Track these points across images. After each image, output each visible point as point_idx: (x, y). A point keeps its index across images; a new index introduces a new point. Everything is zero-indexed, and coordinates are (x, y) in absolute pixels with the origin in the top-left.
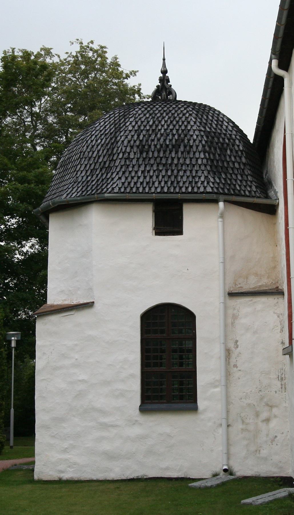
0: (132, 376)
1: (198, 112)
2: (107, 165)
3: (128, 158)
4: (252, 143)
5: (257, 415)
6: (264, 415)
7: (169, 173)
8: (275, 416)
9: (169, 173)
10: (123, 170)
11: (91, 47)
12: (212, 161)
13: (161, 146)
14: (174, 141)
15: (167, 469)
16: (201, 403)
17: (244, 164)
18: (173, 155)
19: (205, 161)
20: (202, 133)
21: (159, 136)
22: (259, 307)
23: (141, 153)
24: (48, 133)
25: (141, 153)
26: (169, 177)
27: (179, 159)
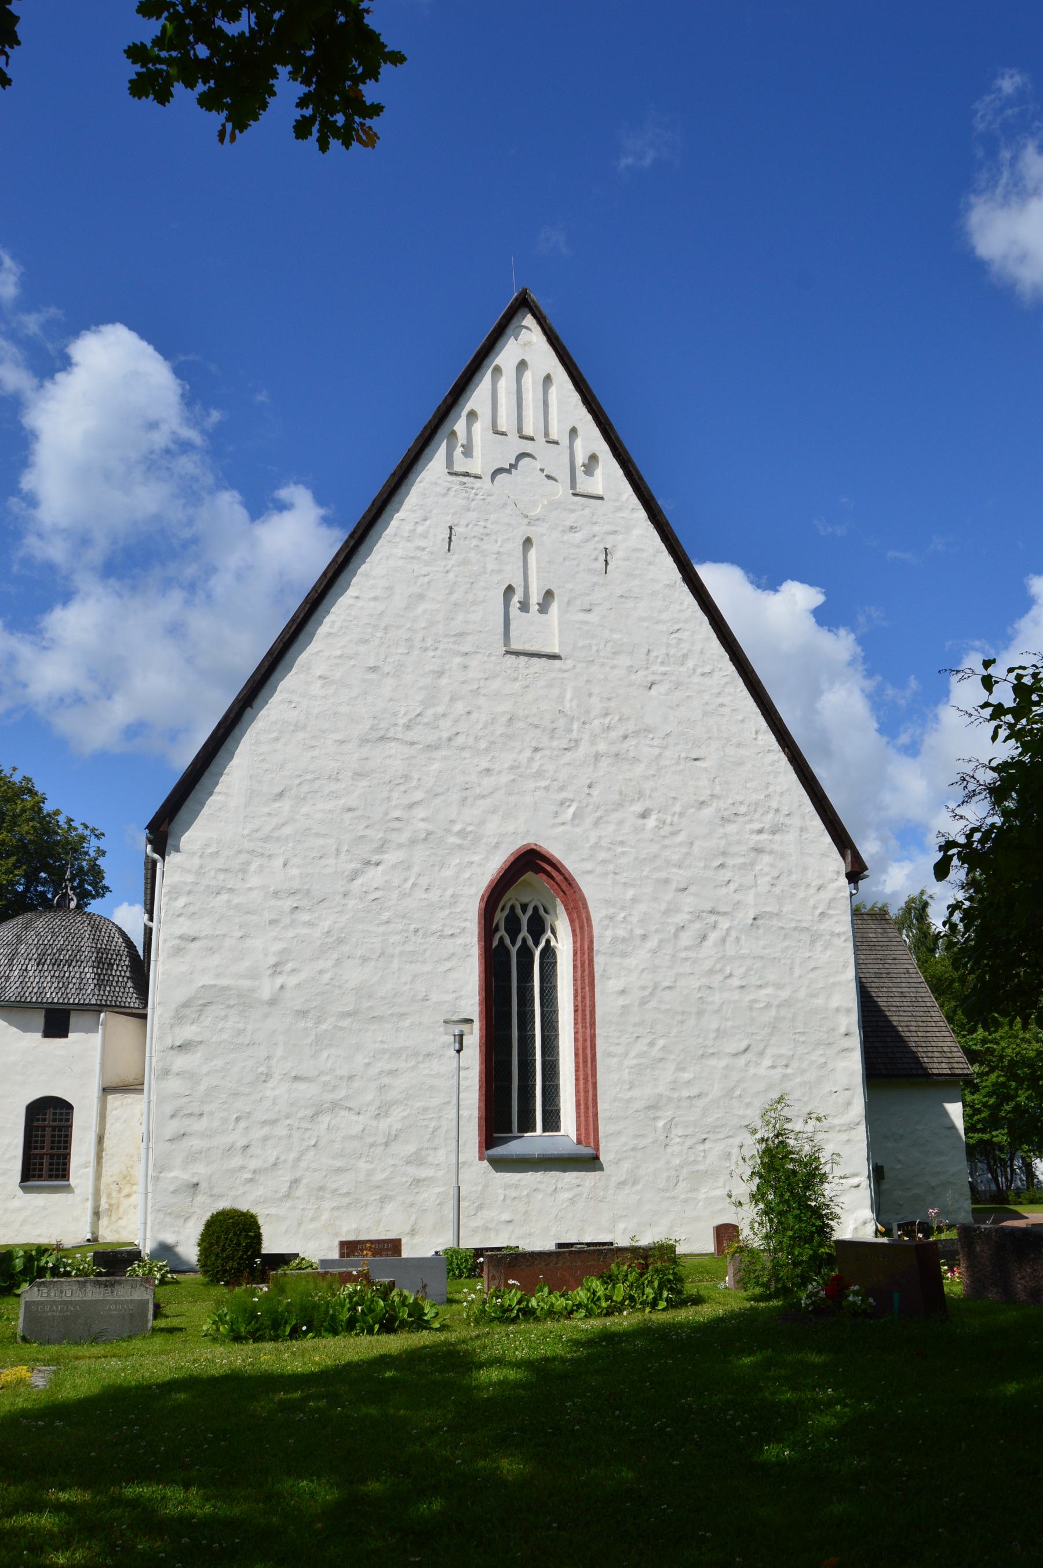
0: (15, 1157)
1: (92, 928)
2: (6, 974)
3: (26, 970)
4: (276, 66)
5: (120, 1191)
6: (125, 1192)
7: (61, 985)
8: (135, 1192)
9: (61, 985)
10: (20, 980)
11: (298, 105)
12: (99, 975)
13: (56, 960)
14: (67, 956)
15: (39, 1236)
16: (73, 1180)
17: (128, 978)
18: (65, 968)
19: (93, 976)
20: (93, 950)
21: (55, 951)
22: (130, 1100)
23: (38, 965)
24: (340, 13)
25: (38, 965)
26: (60, 988)
27: (70, 972)
